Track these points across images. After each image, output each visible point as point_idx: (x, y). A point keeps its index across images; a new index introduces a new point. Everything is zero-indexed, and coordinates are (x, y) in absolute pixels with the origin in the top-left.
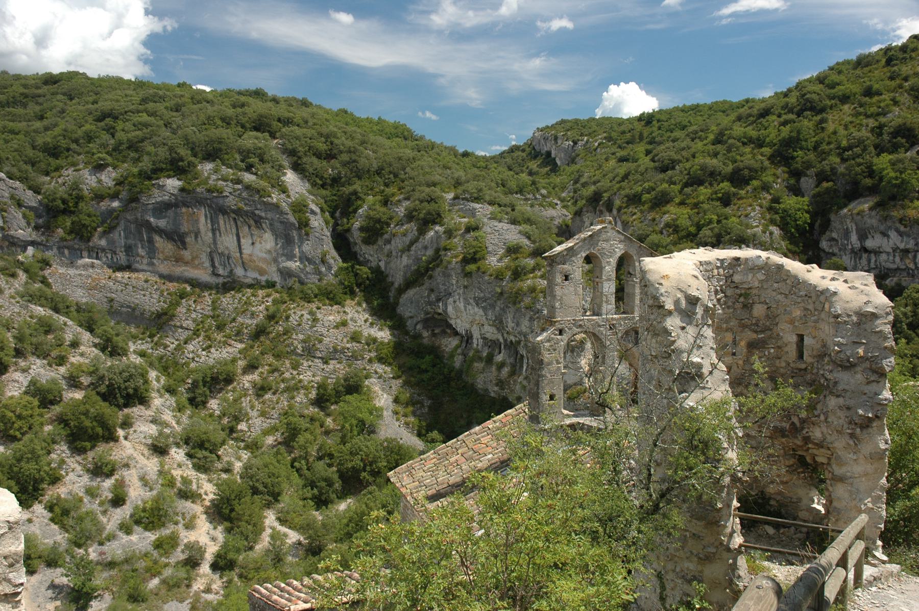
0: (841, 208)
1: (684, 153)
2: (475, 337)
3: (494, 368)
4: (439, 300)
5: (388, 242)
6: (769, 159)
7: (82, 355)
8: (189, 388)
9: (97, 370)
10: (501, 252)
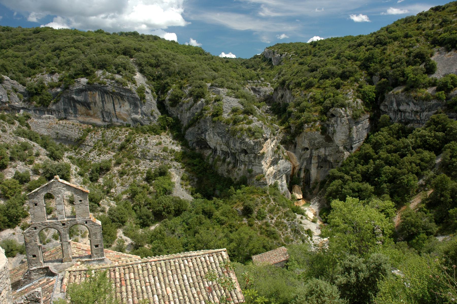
0: (390, 91)
1: (322, 63)
2: (218, 149)
3: (226, 164)
4: (202, 133)
5: (181, 106)
6: (359, 67)
7: (40, 160)
8: (91, 173)
9: (46, 167)
10: (230, 111)
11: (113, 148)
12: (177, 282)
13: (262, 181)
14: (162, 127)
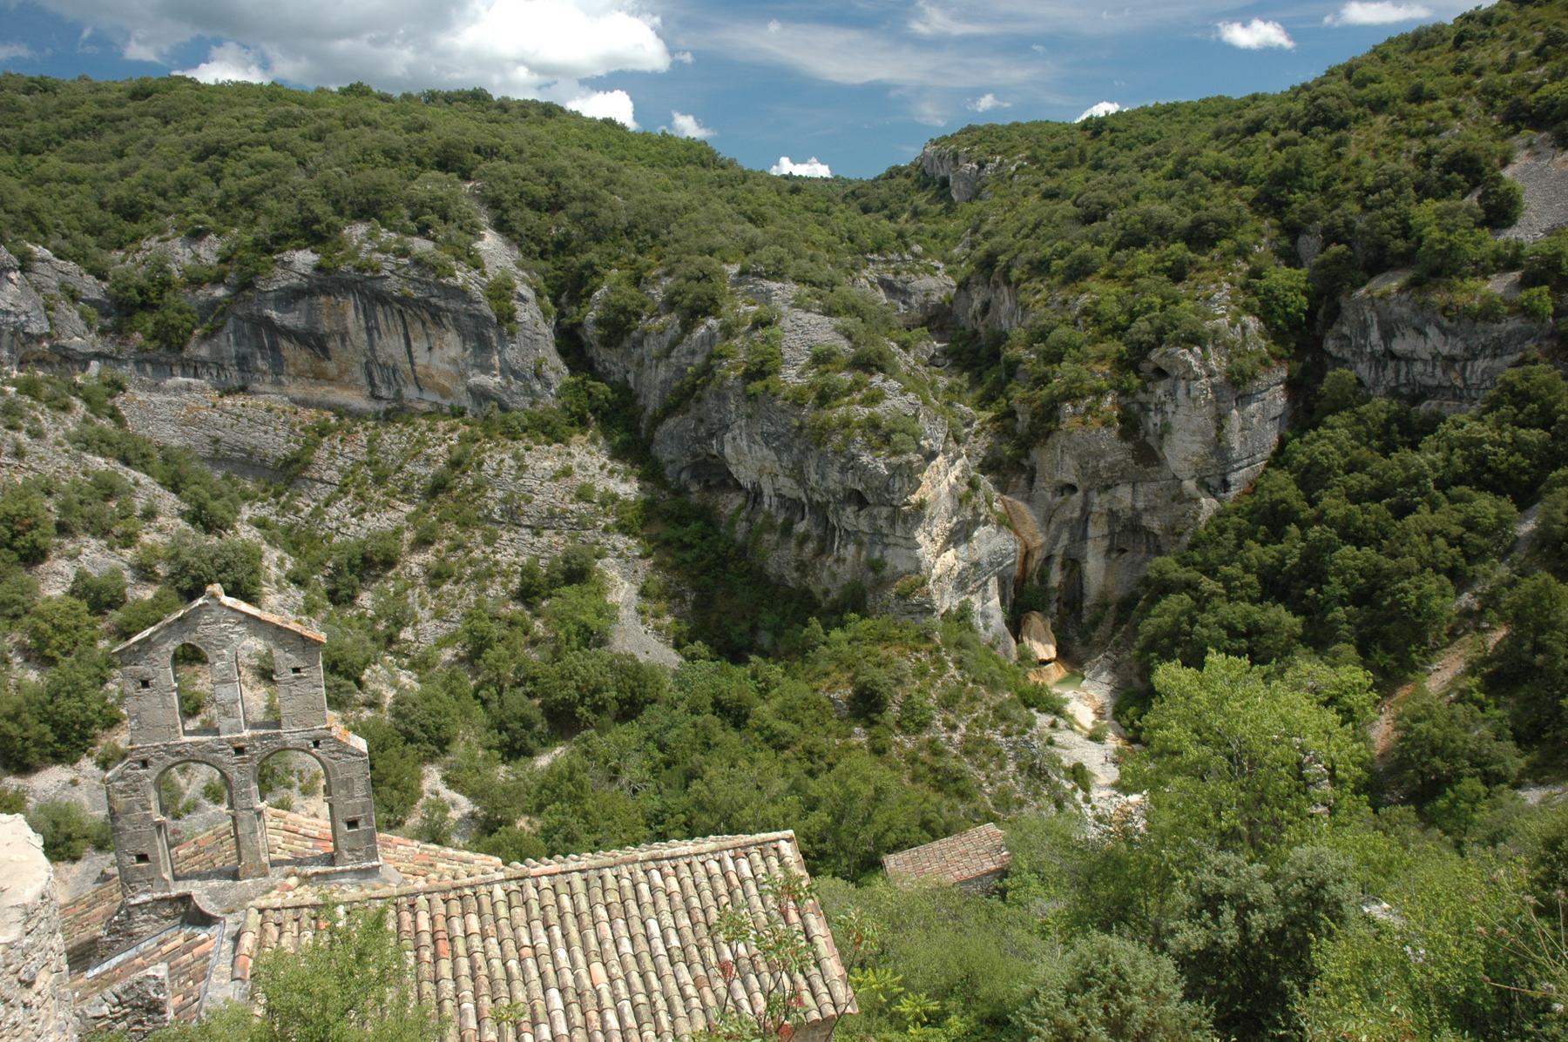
0: (1357, 287)
1: (1122, 193)
3: (793, 543)
4: (711, 435)
5: (639, 343)
6: (1251, 205)
7: (160, 530)
8: (330, 576)
11: (406, 489)
12: (626, 947)
13: (916, 599)
14: (572, 415)
